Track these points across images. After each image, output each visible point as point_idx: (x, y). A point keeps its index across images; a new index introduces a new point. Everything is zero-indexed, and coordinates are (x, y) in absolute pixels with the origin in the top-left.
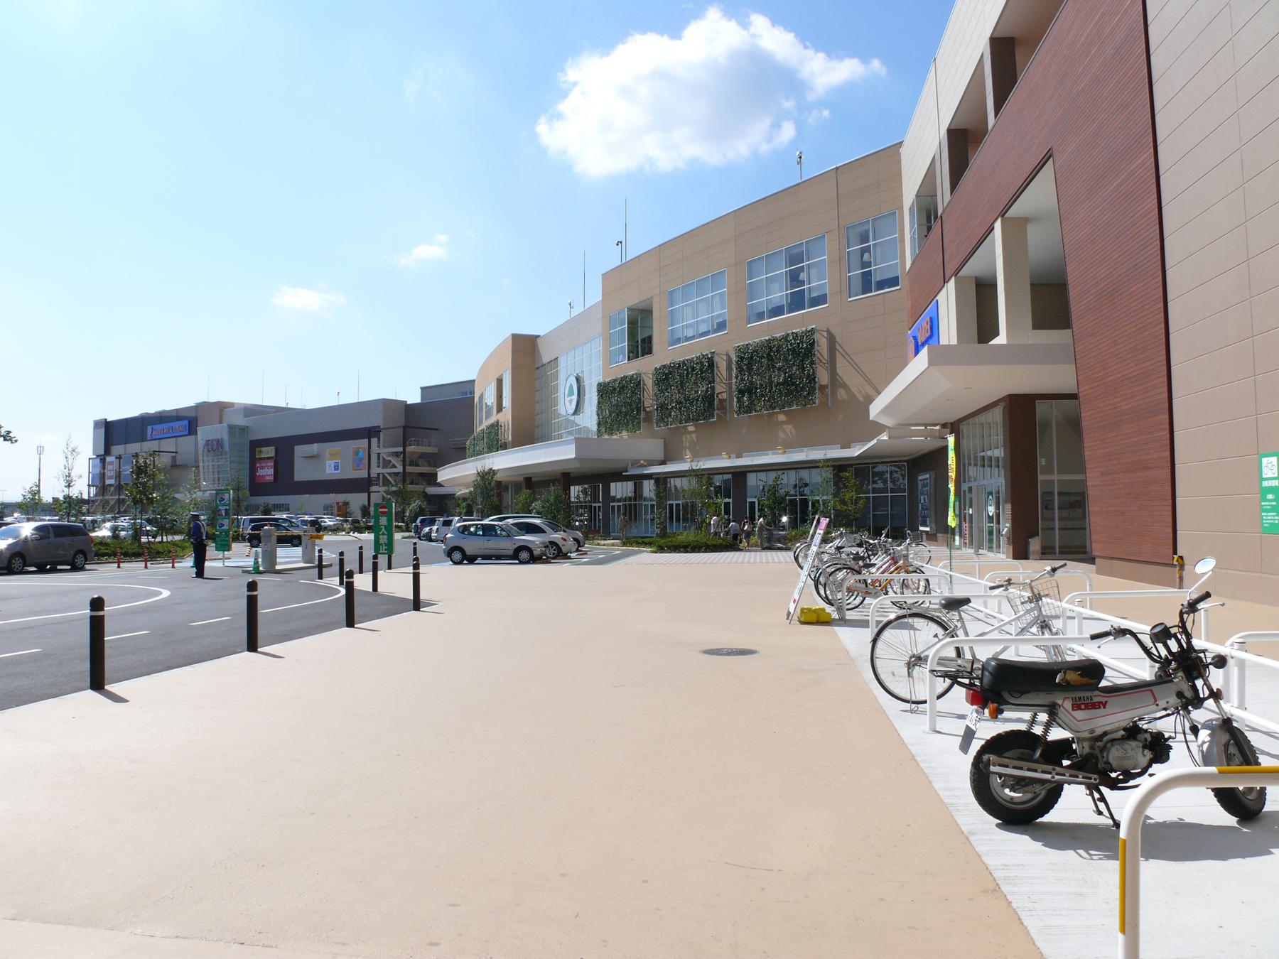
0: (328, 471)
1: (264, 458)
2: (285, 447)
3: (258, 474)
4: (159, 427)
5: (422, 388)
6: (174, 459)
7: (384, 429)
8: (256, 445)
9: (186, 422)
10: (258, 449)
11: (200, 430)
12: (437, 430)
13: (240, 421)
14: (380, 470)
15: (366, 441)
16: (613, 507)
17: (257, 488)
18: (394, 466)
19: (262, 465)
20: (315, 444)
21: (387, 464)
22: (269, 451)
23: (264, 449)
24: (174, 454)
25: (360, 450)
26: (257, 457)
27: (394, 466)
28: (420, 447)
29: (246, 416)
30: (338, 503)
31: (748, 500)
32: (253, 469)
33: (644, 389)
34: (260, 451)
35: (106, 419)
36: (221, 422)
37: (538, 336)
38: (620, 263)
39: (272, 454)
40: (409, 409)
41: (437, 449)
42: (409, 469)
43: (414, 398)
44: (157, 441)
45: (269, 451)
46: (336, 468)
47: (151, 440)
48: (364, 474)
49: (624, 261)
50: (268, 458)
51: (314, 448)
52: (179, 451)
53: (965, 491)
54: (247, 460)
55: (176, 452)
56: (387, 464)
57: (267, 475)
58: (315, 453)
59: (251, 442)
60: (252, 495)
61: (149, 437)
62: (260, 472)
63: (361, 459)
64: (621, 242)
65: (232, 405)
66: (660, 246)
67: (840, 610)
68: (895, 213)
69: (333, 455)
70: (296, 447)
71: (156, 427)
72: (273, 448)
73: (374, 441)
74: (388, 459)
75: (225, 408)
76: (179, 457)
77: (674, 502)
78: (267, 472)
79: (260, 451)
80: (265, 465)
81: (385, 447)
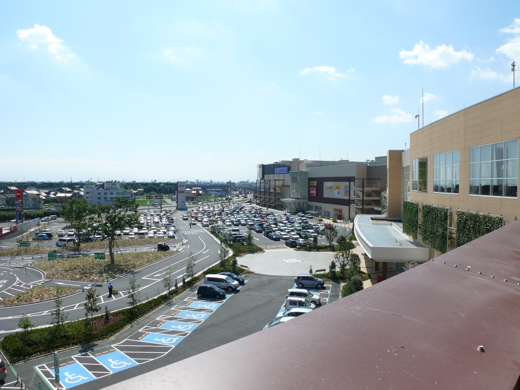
2: (321, 181)
4: (279, 169)
8: (311, 179)
12: (380, 179)
18: (359, 197)
28: (372, 188)
29: (307, 167)
32: (309, 191)
35: (263, 164)
37: (403, 151)
38: (417, 129)
44: (278, 174)
45: (315, 183)
49: (421, 127)
50: (315, 186)
52: (285, 179)
54: (307, 186)
55: (284, 180)
59: (308, 178)
60: (309, 201)
62: (311, 192)
64: (418, 116)
66: (430, 124)
68: (517, 140)
70: (324, 183)
71: (278, 169)
75: (300, 163)
78: (314, 192)
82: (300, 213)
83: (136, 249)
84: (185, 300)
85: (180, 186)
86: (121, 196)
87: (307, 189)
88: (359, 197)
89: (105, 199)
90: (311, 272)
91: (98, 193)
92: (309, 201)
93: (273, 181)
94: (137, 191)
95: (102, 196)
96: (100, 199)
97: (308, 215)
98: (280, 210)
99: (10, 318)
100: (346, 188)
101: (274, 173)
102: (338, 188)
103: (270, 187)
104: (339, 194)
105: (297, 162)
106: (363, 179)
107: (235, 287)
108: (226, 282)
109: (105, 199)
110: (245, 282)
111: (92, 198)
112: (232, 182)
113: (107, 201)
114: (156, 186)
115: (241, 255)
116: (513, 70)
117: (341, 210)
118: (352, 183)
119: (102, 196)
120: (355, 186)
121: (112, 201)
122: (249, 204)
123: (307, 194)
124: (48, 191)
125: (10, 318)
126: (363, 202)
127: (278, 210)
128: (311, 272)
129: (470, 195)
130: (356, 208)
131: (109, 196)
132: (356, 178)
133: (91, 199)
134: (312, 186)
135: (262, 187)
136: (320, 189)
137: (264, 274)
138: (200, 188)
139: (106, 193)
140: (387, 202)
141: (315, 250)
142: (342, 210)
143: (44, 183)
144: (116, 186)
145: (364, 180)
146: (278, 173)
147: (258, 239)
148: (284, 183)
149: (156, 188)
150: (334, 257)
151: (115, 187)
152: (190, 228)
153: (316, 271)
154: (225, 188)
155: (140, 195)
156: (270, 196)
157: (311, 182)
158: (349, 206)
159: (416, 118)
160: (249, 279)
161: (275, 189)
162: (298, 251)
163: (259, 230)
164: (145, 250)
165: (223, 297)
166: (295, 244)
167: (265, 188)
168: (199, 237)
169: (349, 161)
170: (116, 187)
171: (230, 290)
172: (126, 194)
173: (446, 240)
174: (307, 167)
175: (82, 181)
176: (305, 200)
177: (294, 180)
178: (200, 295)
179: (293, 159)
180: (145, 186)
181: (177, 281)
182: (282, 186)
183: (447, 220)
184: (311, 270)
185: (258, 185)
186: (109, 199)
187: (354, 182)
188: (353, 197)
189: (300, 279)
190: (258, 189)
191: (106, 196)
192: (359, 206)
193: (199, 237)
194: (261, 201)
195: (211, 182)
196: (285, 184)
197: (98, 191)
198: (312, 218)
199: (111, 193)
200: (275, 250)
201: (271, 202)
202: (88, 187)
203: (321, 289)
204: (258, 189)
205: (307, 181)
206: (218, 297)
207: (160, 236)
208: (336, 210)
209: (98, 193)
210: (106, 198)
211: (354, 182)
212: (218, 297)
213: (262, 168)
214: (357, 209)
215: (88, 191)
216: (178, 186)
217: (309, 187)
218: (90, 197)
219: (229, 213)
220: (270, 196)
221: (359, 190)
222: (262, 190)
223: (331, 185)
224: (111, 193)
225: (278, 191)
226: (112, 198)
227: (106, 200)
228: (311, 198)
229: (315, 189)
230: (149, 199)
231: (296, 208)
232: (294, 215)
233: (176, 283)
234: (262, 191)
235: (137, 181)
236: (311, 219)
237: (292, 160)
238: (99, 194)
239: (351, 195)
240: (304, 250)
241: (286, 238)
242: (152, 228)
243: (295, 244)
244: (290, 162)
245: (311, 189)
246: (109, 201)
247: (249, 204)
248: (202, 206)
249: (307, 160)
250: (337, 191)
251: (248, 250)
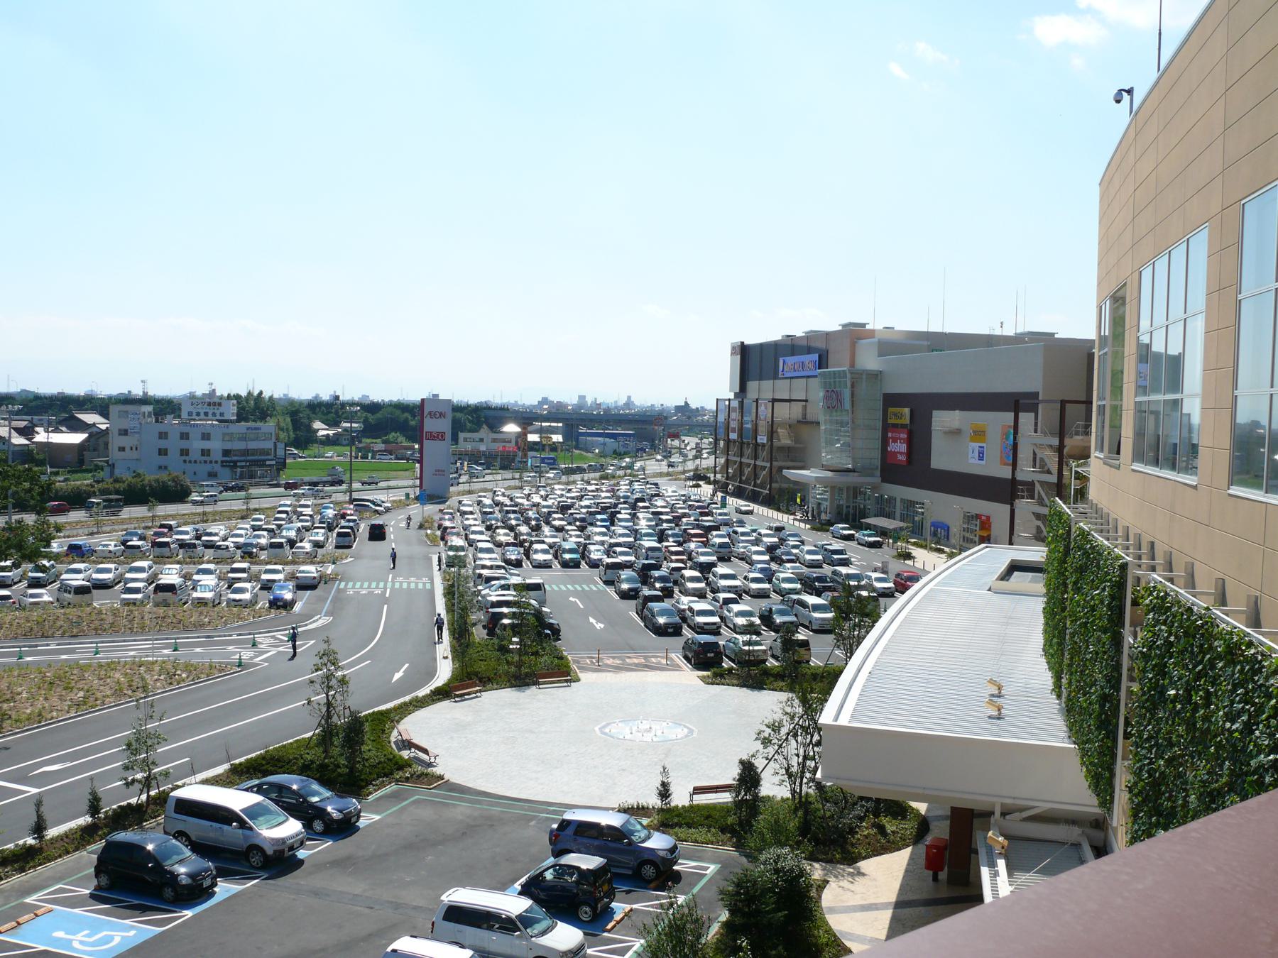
3: (889, 449)
8: (892, 400)
15: (1010, 416)
18: (1049, 472)
24: (804, 403)
35: (742, 343)
47: (783, 378)
48: (1006, 473)
54: (879, 424)
55: (806, 401)
57: (899, 452)
59: (884, 394)
60: (885, 480)
62: (892, 447)
64: (1130, 92)
67: (511, 499)
70: (935, 413)
71: (787, 359)
82: (840, 526)
83: (97, 648)
84: (28, 900)
85: (430, 413)
86: (240, 446)
87: (879, 434)
88: (1049, 472)
89: (182, 455)
90: (664, 792)
91: (160, 434)
92: (883, 481)
93: (765, 404)
94: (340, 430)
95: (174, 444)
96: (166, 454)
97: (864, 535)
98: (783, 512)
100: (1006, 435)
101: (775, 376)
102: (979, 434)
103: (756, 424)
104: (981, 458)
105: (854, 333)
106: (1063, 403)
107: (275, 852)
108: (243, 824)
109: (182, 455)
110: (362, 823)
111: (136, 449)
112: (693, 405)
113: (190, 462)
114: (406, 415)
115: (469, 694)
117: (988, 518)
118: (1026, 419)
119: (174, 444)
120: (1036, 431)
121: (205, 462)
122: (691, 487)
124: (26, 423)
127: (779, 510)
128: (664, 792)
129: (1235, 490)
130: (1033, 513)
131: (197, 445)
132: (1040, 398)
133: (135, 455)
134: (895, 426)
135: (733, 424)
136: (919, 437)
137: (483, 789)
138: (560, 425)
139: (187, 434)
141: (781, 684)
142: (991, 520)
143: (38, 397)
144: (222, 409)
145: (1068, 406)
146: (787, 375)
147: (600, 626)
148: (808, 410)
149: (406, 420)
150: (757, 739)
151: (218, 413)
152: (394, 568)
153: (695, 789)
154: (647, 427)
155: (345, 442)
156: (756, 459)
157: (891, 410)
158: (1012, 505)
159: (1118, 101)
160: (385, 814)
161: (772, 433)
162: (712, 684)
163: (630, 590)
164: (132, 653)
165: (196, 892)
166: (712, 655)
167: (741, 430)
168: (386, 606)
169: (1056, 336)
170: (222, 414)
171: (256, 859)
172: (257, 439)
173: (1115, 740)
174: (880, 355)
175: (437, 395)
176: (872, 475)
177: (833, 400)
178: (104, 880)
179: (844, 326)
180: (369, 415)
181: (42, 809)
182: (799, 422)
183: (1123, 626)
184: (665, 785)
185: (721, 418)
186: (195, 455)
187: (1033, 414)
188: (1026, 471)
189: (570, 831)
190: (721, 430)
191: (184, 444)
193: (386, 606)
194: (730, 475)
195: (129, 392)
196: (809, 417)
197: (161, 427)
198: (880, 547)
199: (203, 434)
200: (629, 674)
201: (759, 482)
202: (127, 412)
203: (652, 885)
204: (721, 430)
205: (880, 405)
206: (168, 893)
207: (234, 600)
208: (970, 518)
209: (160, 434)
210: (184, 452)
211: (1033, 414)
212: (168, 893)
213: (739, 357)
214: (1038, 516)
215: (123, 427)
216: (425, 414)
217: (886, 427)
218: (131, 449)
219: (578, 516)
220: (756, 458)
221: (1051, 446)
222: (733, 436)
223: (956, 425)
224: (203, 434)
225: (784, 439)
226: (205, 452)
227: (184, 458)
228: (890, 471)
229: (904, 436)
230: (362, 458)
231: (839, 507)
232: (819, 533)
233: (39, 817)
234: (734, 441)
235: (345, 397)
236: (873, 551)
237: (840, 328)
238: (163, 435)
239: (1019, 462)
240: (735, 682)
241: (706, 627)
242: (236, 565)
243: (712, 655)
244: (827, 334)
245: (890, 435)
246: (195, 462)
247: (691, 487)
248: (503, 490)
249: (893, 328)
250: (976, 445)
251: (507, 673)
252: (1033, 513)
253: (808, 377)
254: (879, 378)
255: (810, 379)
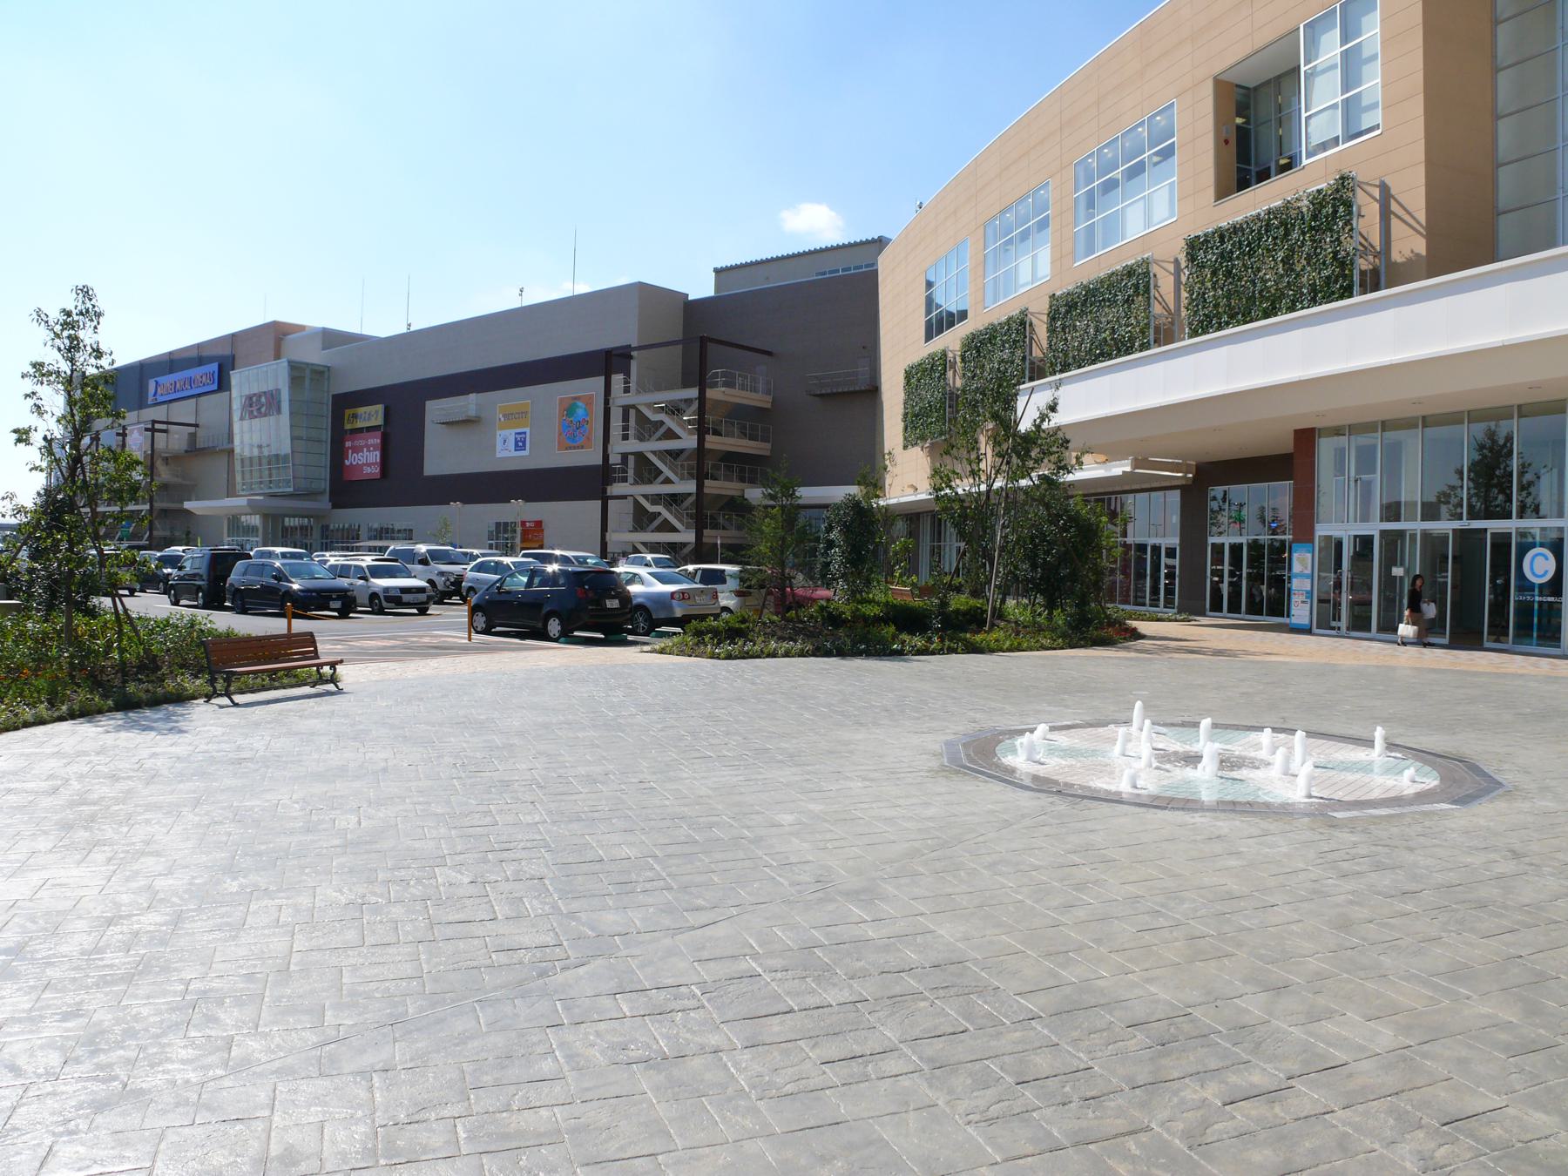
0: (500, 453)
1: (360, 430)
3: (347, 463)
4: (167, 380)
5: (718, 271)
6: (193, 436)
7: (639, 348)
8: (346, 402)
9: (214, 367)
10: (348, 412)
11: (235, 377)
12: (769, 353)
13: (314, 356)
14: (633, 445)
16: (1218, 549)
17: (346, 490)
18: (670, 435)
19: (357, 443)
20: (472, 396)
21: (647, 428)
22: (372, 415)
23: (361, 410)
24: (192, 429)
25: (580, 404)
26: (348, 427)
27: (670, 435)
30: (523, 523)
31: (1211, 540)
33: (1032, 338)
34: (355, 416)
36: (277, 356)
39: (378, 420)
40: (693, 310)
41: (769, 398)
42: (712, 442)
43: (701, 287)
45: (372, 415)
46: (520, 444)
48: (592, 457)
50: (369, 429)
51: (470, 403)
53: (323, 556)
54: (327, 435)
55: (196, 426)
56: (647, 428)
58: (472, 413)
59: (334, 396)
60: (336, 506)
61: (150, 400)
62: (353, 459)
63: (581, 424)
65: (301, 328)
69: (511, 417)
70: (427, 403)
71: (161, 379)
72: (380, 408)
73: (617, 379)
74: (654, 417)
76: (201, 433)
77: (1227, 540)
78: (366, 459)
79: (355, 416)
80: (362, 442)
81: (642, 389)
99: (1536, 620)
116: (521, 295)
123: (326, 473)
125: (1536, 620)
126: (701, 464)
130: (680, 438)
140: (1201, 335)
146: (160, 399)
182: (186, 451)
192: (668, 481)
205: (327, 410)
252: (680, 438)
253: (199, 395)
254: (326, 376)
255: (172, 405)
